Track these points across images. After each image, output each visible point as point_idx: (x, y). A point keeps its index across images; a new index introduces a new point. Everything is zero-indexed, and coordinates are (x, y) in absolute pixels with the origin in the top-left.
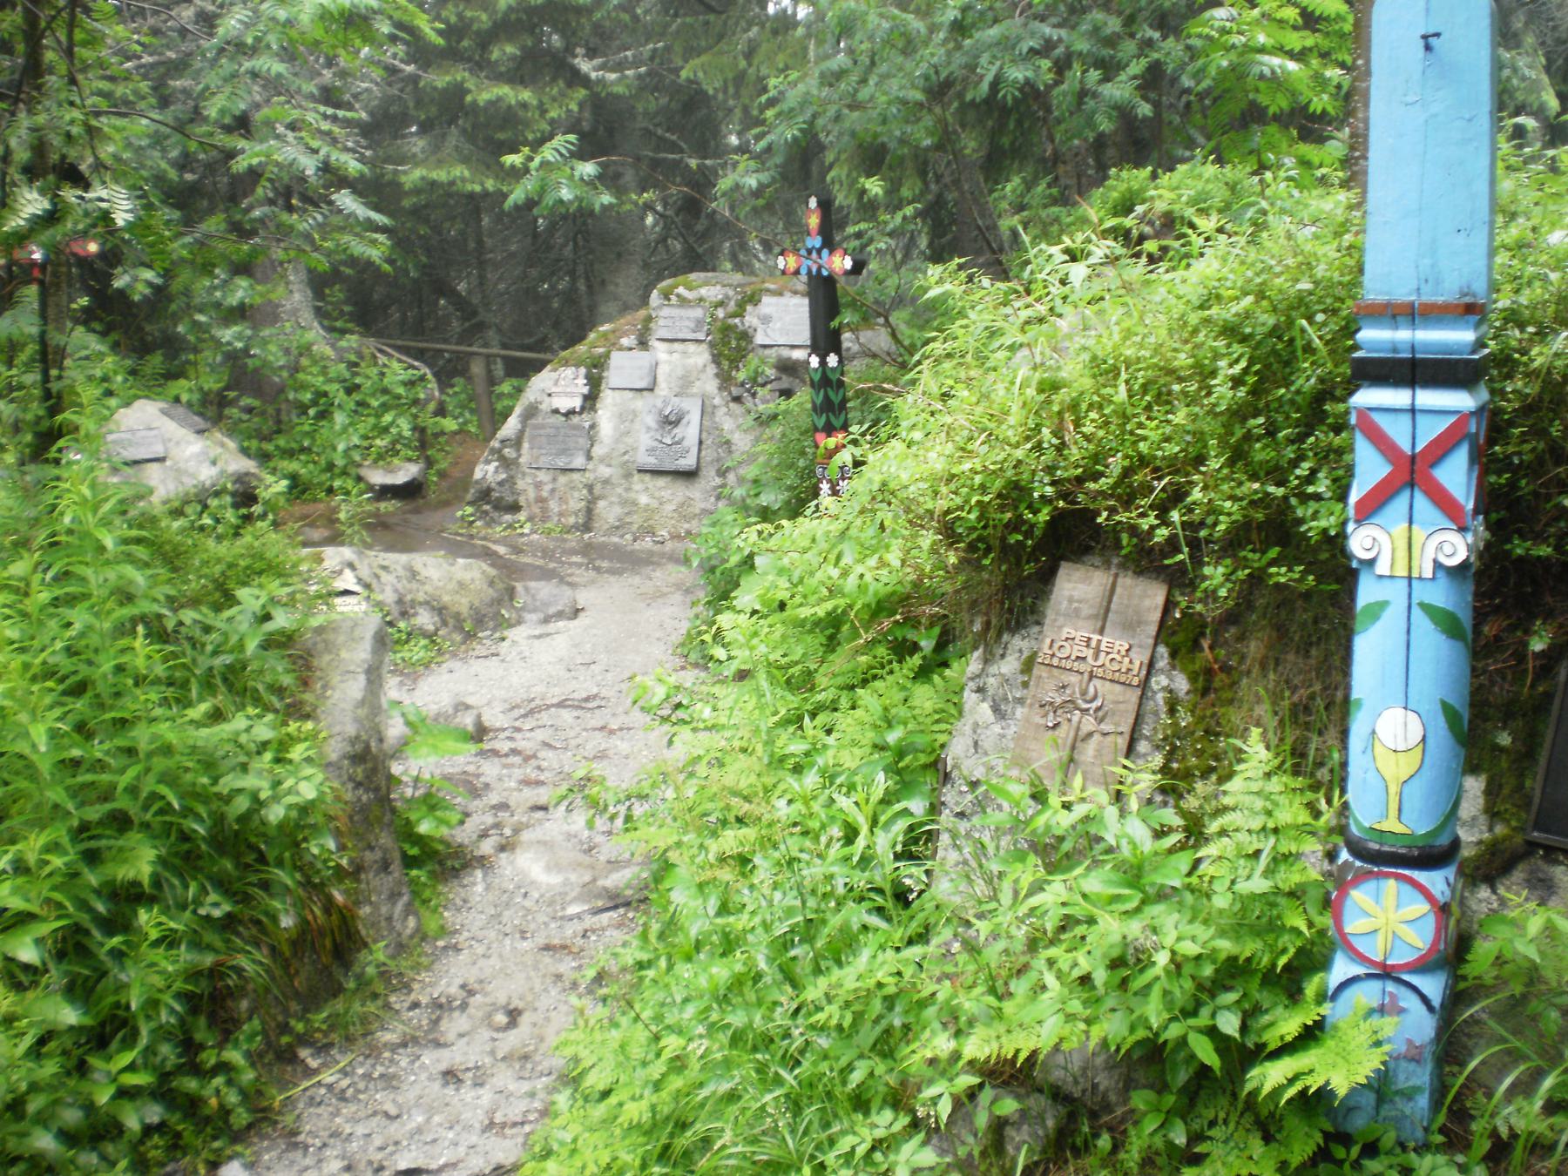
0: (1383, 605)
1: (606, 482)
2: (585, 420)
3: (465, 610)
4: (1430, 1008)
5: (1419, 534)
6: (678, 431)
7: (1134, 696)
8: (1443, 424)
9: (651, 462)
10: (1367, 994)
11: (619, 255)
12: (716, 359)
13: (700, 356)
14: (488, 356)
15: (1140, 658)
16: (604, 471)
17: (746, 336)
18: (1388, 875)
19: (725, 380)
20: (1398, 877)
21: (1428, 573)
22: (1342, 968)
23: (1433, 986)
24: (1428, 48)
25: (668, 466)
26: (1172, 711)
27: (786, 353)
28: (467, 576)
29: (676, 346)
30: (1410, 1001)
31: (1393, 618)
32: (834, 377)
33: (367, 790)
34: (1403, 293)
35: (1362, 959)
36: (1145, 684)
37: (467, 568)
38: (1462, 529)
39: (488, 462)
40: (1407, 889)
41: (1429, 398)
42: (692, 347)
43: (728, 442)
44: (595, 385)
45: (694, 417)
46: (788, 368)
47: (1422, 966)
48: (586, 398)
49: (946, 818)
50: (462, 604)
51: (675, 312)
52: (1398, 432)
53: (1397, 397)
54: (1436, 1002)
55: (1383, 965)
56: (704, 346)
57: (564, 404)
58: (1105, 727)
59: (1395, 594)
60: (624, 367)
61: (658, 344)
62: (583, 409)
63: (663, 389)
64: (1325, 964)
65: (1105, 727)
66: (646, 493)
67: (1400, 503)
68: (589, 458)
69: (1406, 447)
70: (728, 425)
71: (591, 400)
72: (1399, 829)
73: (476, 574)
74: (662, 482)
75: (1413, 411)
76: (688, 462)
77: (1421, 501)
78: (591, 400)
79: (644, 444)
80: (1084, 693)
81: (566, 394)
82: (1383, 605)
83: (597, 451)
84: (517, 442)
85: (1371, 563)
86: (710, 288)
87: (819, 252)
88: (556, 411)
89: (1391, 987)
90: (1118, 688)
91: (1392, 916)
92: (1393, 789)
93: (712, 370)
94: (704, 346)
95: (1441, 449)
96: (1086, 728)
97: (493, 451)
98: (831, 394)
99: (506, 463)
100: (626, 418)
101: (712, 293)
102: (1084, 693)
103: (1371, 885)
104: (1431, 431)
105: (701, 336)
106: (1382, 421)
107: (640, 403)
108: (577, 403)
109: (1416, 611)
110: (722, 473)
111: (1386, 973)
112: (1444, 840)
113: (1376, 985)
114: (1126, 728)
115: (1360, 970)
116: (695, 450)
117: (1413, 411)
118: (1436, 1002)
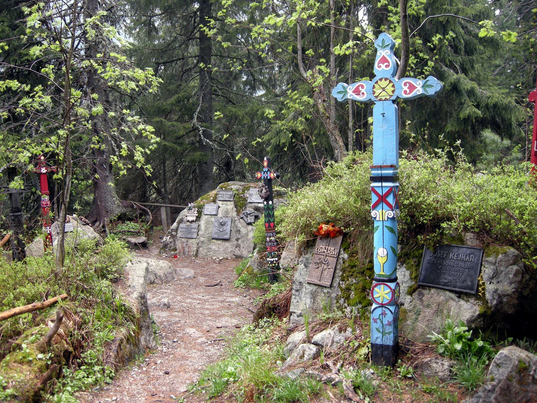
0: (378, 226)
1: (203, 242)
2: (194, 225)
3: (162, 275)
4: (392, 313)
5: (384, 211)
6: (224, 227)
7: (335, 260)
8: (388, 189)
9: (216, 236)
10: (379, 311)
11: (206, 178)
12: (236, 206)
13: (230, 206)
14: (166, 207)
15: (337, 251)
16: (202, 239)
17: (245, 200)
18: (381, 284)
19: (238, 212)
20: (384, 284)
21: (386, 219)
22: (374, 306)
23: (392, 308)
24: (383, 116)
25: (221, 238)
26: (344, 263)
27: (257, 205)
28: (163, 265)
29: (224, 202)
30: (388, 312)
31: (380, 228)
32: (271, 207)
33: (144, 307)
34: (380, 164)
35: (378, 303)
36: (338, 257)
37: (164, 263)
38: (392, 210)
39: (167, 236)
40: (386, 287)
41: (385, 184)
42: (229, 203)
43: (239, 231)
44: (200, 213)
45: (230, 223)
46: (257, 209)
47: (389, 304)
48: (197, 217)
49: (293, 292)
50: (161, 273)
51: (224, 193)
52: (379, 191)
53: (379, 184)
54: (393, 312)
55: (382, 304)
56: (232, 203)
57: (190, 219)
58: (329, 267)
59: (380, 224)
60: (209, 208)
61: (218, 202)
62: (196, 220)
63: (220, 215)
64: (371, 305)
65: (329, 267)
66: (215, 246)
67: (380, 206)
68: (198, 235)
69: (381, 194)
70: (239, 225)
71: (198, 218)
72: (383, 274)
73: (165, 265)
74: (219, 242)
75: (382, 187)
76: (227, 237)
77: (385, 205)
78: (198, 218)
79: (214, 230)
80: (324, 260)
81: (191, 216)
82: (378, 226)
83: (201, 233)
84: (176, 230)
85: (375, 218)
86: (235, 186)
87: (267, 172)
88: (188, 221)
89: (384, 309)
90: (332, 258)
91: (383, 293)
92: (382, 265)
93: (235, 209)
94: (232, 203)
95: (388, 194)
96: (325, 268)
97: (169, 233)
98: (270, 212)
99: (173, 236)
100: (207, 222)
101: (234, 187)
102: (324, 260)
103: (378, 286)
104: (385, 190)
105: (232, 200)
106: (376, 189)
107: (213, 219)
108: (194, 218)
109: (384, 227)
110: (237, 240)
111: (382, 306)
112: (393, 277)
113: (381, 309)
114: (334, 267)
115: (377, 306)
116: (229, 233)
117: (382, 187)
118: (393, 312)
